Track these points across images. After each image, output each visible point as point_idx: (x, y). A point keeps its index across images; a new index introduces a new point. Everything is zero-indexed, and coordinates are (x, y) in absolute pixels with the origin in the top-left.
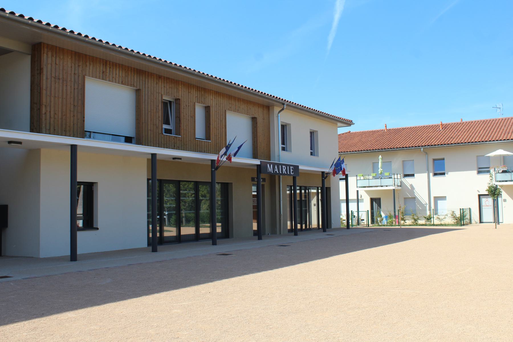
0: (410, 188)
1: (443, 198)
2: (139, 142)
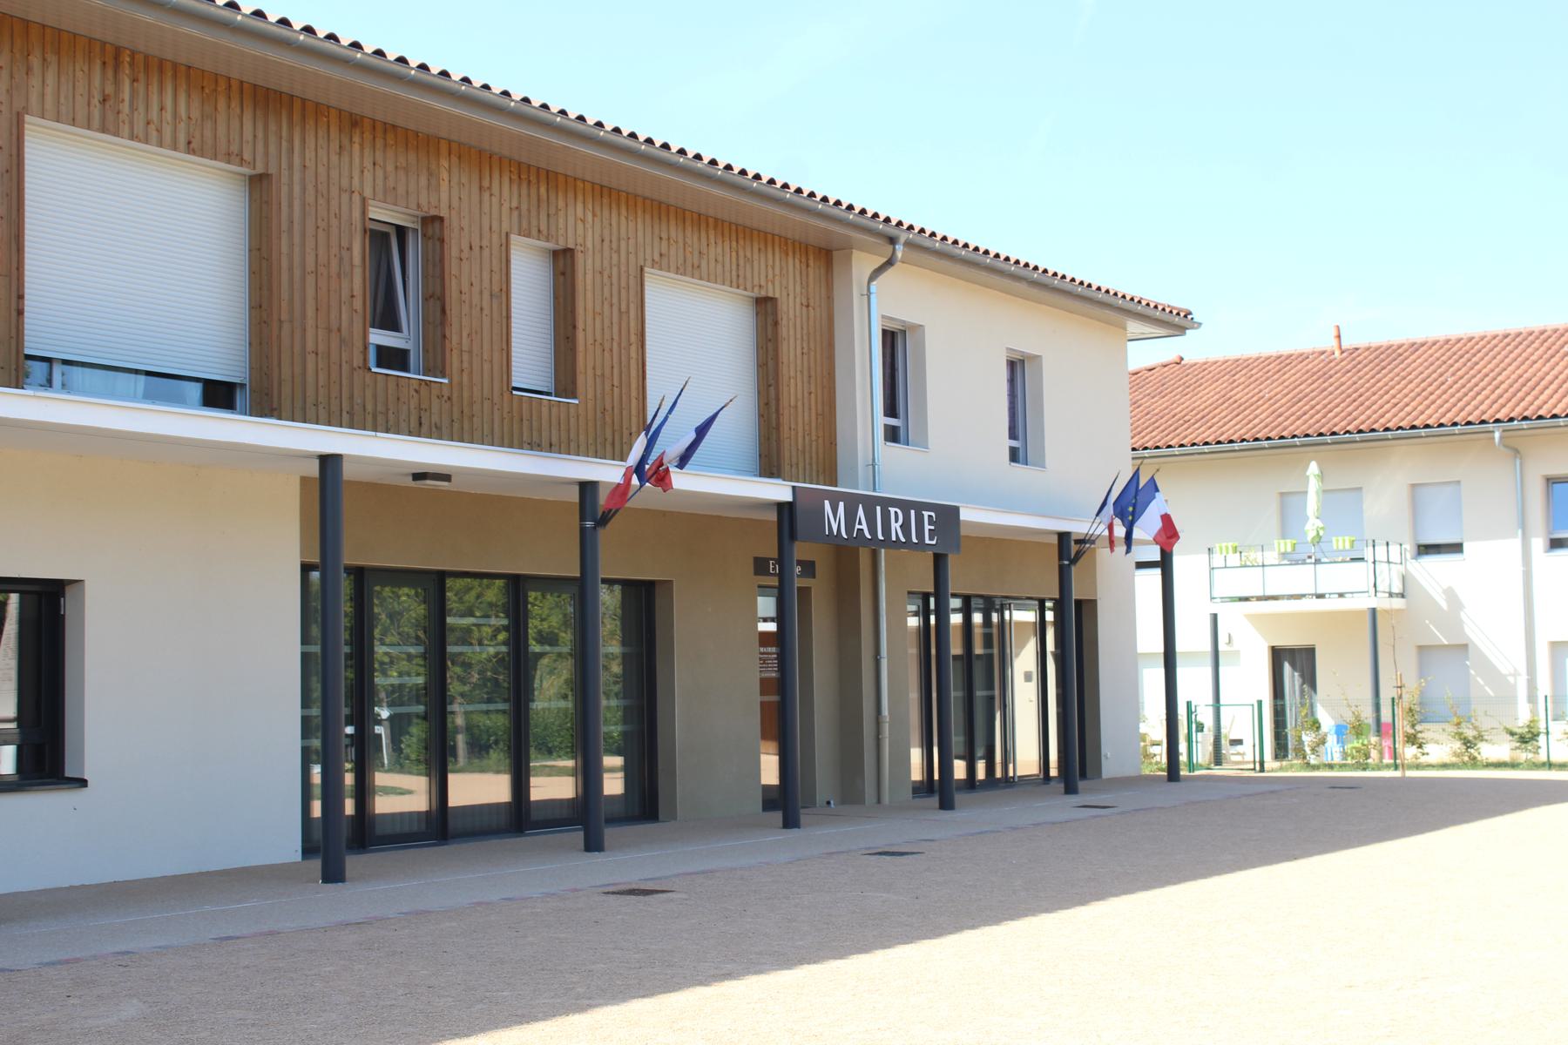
2: (266, 407)
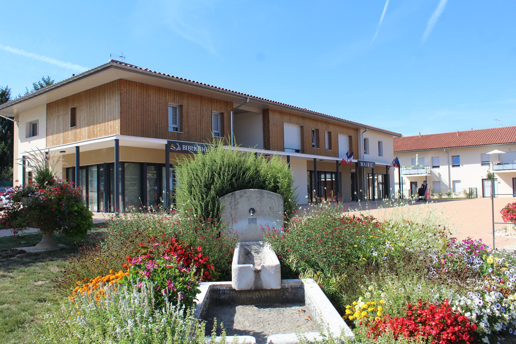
0: (438, 176)
1: (459, 181)
2: (303, 152)
